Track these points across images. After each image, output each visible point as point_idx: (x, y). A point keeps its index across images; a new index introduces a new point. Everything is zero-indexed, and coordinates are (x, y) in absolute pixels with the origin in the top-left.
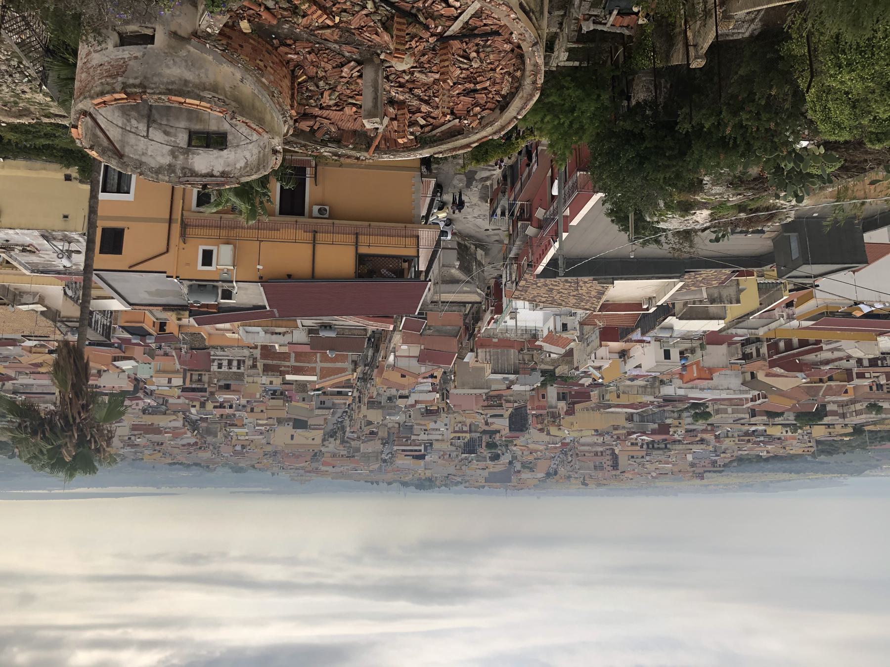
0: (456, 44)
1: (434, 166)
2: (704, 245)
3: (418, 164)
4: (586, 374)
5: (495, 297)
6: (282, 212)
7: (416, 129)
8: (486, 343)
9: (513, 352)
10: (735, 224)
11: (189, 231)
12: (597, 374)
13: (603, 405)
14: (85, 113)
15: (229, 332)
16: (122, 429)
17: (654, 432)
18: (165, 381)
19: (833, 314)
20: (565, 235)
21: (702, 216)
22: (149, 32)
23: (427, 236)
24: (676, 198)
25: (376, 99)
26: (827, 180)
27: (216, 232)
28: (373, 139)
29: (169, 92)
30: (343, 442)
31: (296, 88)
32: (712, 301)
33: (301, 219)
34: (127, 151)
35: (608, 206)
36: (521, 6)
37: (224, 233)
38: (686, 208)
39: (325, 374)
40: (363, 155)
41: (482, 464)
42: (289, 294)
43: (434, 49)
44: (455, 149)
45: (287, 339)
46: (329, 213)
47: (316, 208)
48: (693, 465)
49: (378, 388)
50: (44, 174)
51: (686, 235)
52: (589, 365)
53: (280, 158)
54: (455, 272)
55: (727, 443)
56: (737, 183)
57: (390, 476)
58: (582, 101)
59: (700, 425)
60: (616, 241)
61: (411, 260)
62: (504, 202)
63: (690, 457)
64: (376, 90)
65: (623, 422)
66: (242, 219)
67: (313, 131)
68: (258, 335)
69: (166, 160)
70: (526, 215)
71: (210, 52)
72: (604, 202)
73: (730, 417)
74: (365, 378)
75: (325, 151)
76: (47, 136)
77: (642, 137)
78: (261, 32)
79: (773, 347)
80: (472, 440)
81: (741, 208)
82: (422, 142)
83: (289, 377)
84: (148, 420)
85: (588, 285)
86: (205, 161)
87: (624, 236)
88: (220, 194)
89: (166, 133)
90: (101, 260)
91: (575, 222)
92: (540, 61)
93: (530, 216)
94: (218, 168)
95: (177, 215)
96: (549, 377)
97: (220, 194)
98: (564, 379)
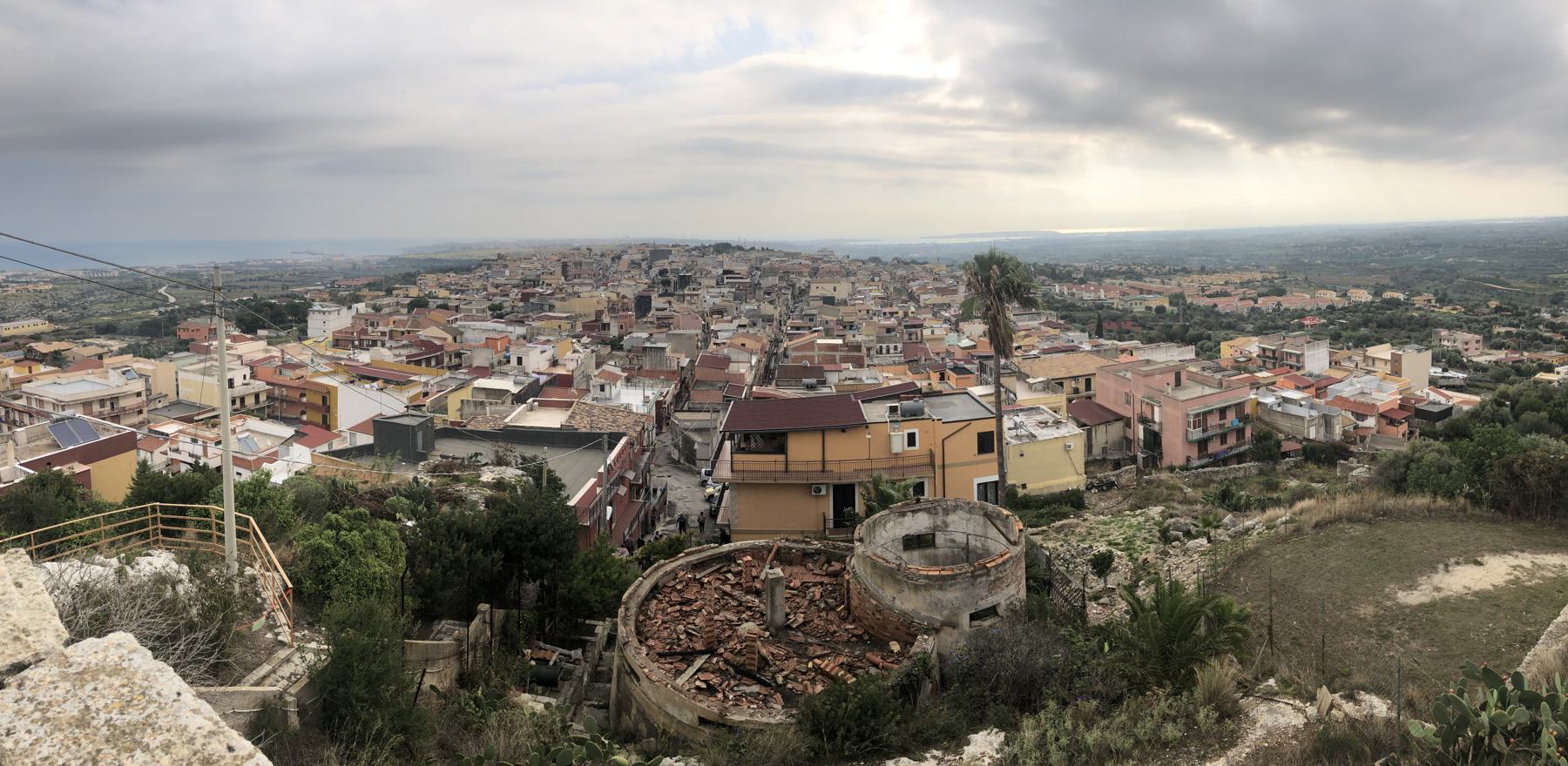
0: (699, 646)
1: (718, 534)
2: (487, 450)
3: (733, 537)
4: (585, 346)
5: (662, 416)
6: (852, 486)
7: (735, 569)
8: (670, 375)
9: (647, 367)
10: (462, 467)
11: (927, 460)
12: (577, 347)
13: (572, 319)
14: (1015, 544)
15: (890, 376)
16: (962, 294)
17: (533, 295)
18: (937, 332)
19: (398, 383)
20: (602, 470)
21: (487, 476)
22: (975, 623)
23: (724, 472)
24: (507, 494)
25: (772, 596)
26: (395, 491)
27: (907, 462)
28: (775, 558)
29: (953, 577)
30: (793, 286)
31: (845, 598)
32: (482, 403)
33: (837, 482)
34: (980, 519)
35: (564, 494)
36: (638, 679)
37: (900, 463)
38: (499, 485)
39: (811, 345)
40: (783, 543)
41: (674, 266)
42: (841, 416)
43: (720, 642)
44: (700, 551)
45: (844, 375)
46: (811, 489)
47: (823, 492)
48: (506, 266)
49: (765, 333)
50: (1041, 485)
51: (500, 462)
52: (583, 353)
53: (856, 535)
54: (697, 438)
55: (477, 285)
56: (459, 501)
57: (753, 255)
58: (584, 589)
59: (497, 300)
60: (558, 462)
61: (737, 450)
62: (654, 501)
63: (507, 273)
64: (773, 603)
65: (557, 304)
66: (885, 477)
67: (829, 562)
68: (867, 377)
69: (951, 518)
70: (635, 489)
71: (924, 618)
72: (568, 498)
73: (474, 307)
74: (776, 342)
75: (817, 545)
76: (1042, 516)
77: (534, 551)
78: (880, 644)
79: (439, 362)
80: (682, 288)
81: (457, 479)
82: (730, 558)
83: (840, 341)
84: (946, 299)
85: (583, 425)
86: (919, 523)
87: (551, 466)
88: (905, 495)
89: (953, 541)
90: (990, 426)
91: (593, 481)
92: (621, 628)
93: (633, 488)
94: (909, 518)
95: (939, 472)
96: (616, 345)
97: (905, 495)
98: (604, 342)
